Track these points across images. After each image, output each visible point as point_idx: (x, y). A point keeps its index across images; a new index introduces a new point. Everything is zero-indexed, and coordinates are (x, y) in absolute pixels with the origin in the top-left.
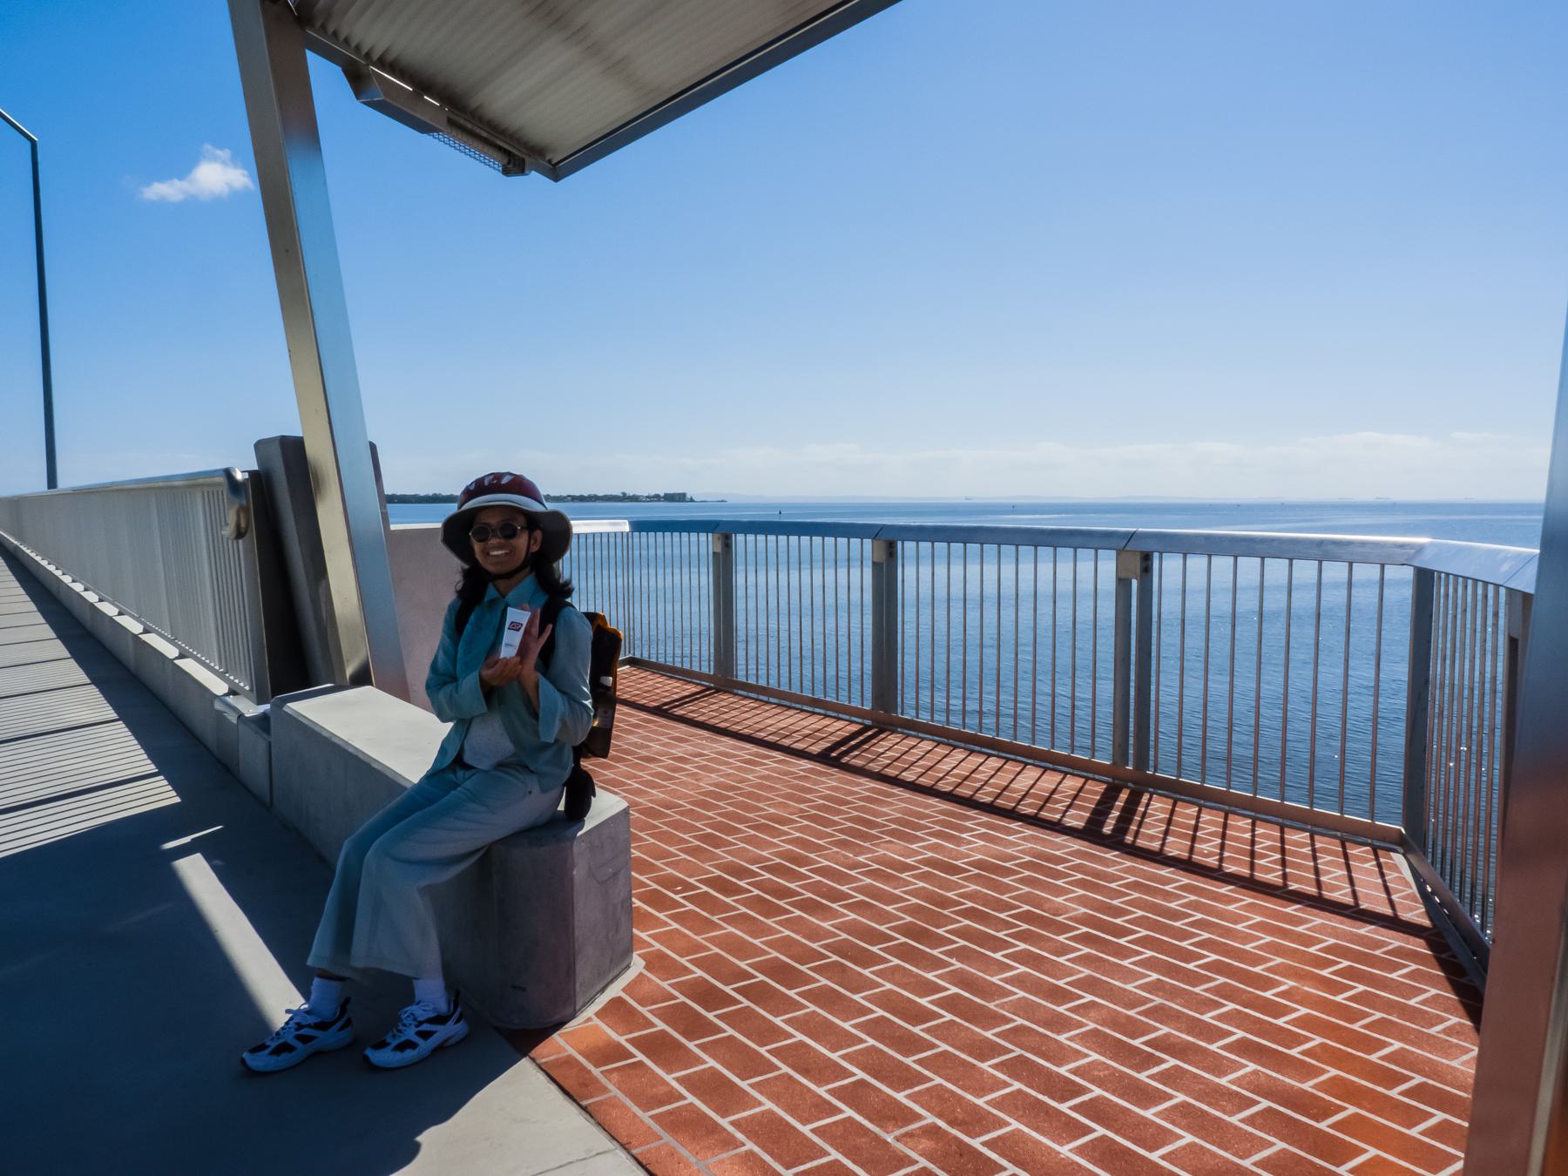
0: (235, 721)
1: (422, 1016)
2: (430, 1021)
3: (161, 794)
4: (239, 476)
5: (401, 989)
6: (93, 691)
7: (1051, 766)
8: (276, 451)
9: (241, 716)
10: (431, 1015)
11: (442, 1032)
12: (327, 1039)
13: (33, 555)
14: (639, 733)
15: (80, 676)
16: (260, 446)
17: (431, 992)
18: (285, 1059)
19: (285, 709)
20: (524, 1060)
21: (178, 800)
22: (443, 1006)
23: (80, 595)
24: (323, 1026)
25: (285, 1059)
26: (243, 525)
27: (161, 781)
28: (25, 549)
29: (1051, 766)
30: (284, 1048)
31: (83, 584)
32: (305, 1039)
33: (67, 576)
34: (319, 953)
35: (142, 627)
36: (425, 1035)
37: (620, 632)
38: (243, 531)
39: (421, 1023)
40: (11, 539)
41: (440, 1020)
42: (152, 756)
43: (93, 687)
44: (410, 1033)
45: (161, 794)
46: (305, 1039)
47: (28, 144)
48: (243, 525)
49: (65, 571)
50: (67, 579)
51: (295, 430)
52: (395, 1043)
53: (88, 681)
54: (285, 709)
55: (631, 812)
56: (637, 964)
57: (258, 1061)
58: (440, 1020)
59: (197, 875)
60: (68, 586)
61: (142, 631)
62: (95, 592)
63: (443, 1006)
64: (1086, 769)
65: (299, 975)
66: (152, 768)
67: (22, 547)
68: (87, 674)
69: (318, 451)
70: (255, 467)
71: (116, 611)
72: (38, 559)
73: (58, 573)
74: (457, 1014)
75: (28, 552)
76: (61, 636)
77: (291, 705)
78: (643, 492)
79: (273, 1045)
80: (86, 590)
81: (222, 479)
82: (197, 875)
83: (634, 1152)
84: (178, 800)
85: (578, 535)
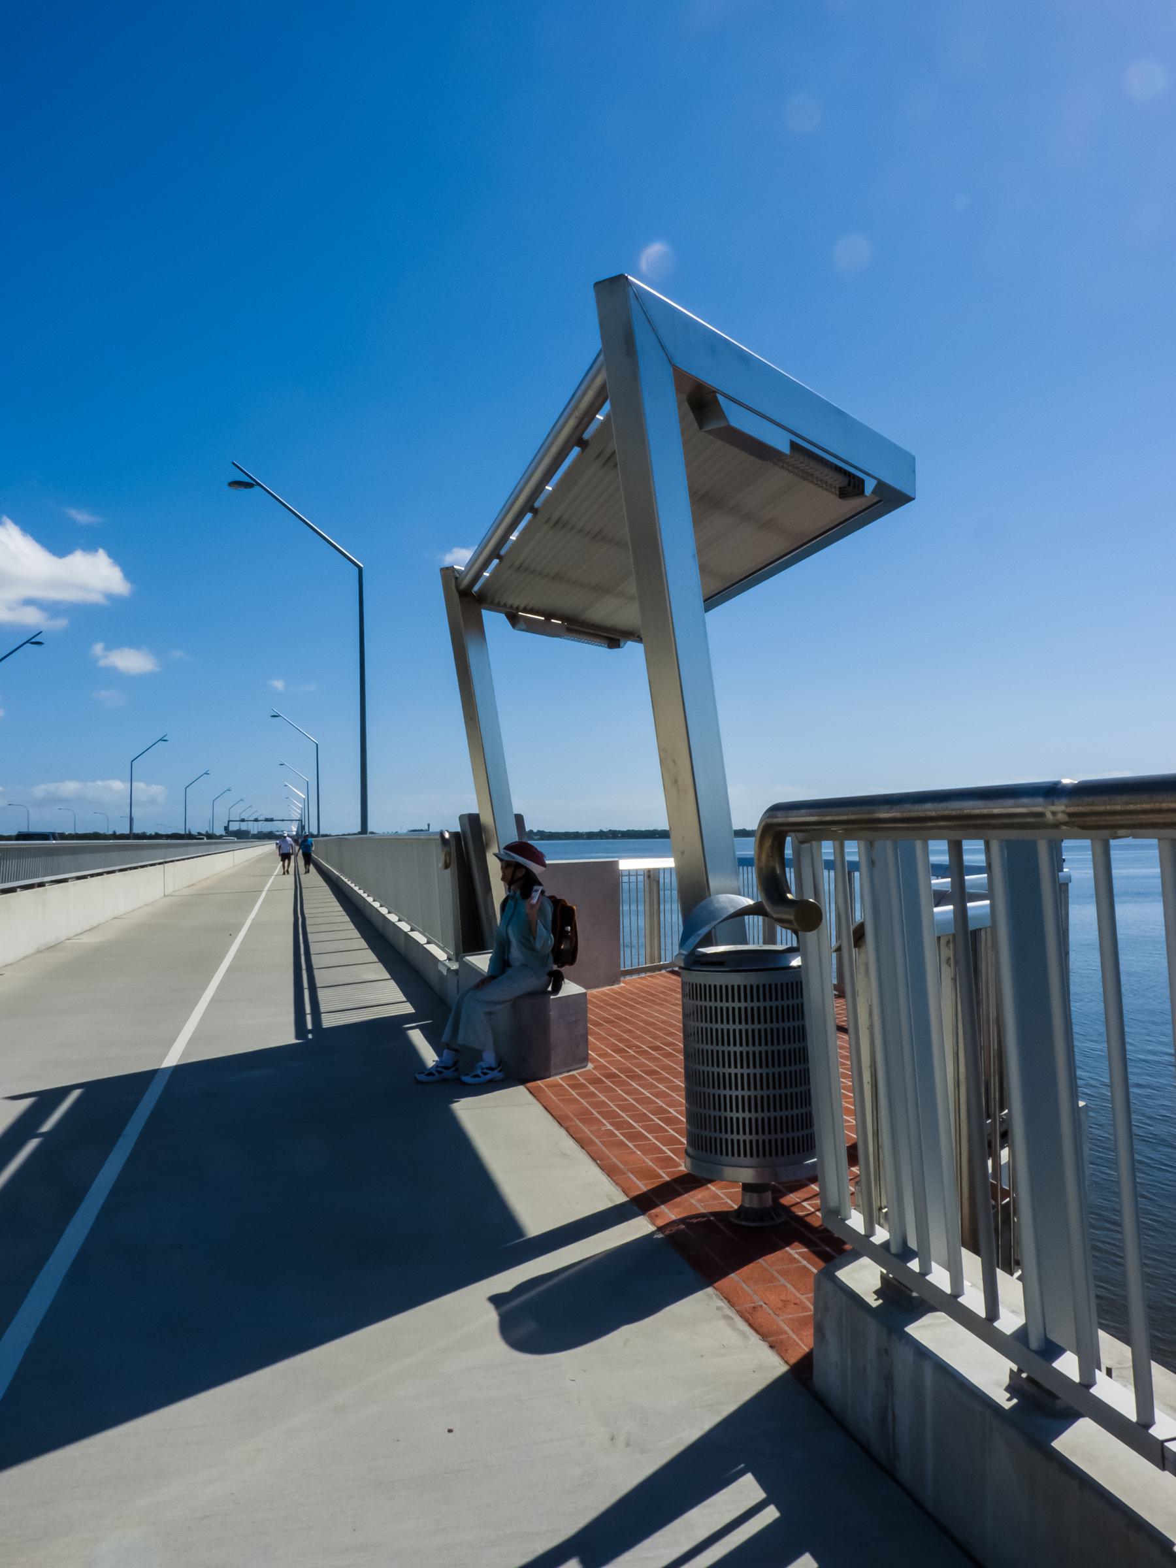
0: (445, 974)
1: (484, 1066)
2: (488, 1068)
3: (408, 1009)
4: (447, 835)
5: (477, 1055)
6: (380, 966)
8: (466, 821)
9: (449, 969)
10: (487, 1066)
11: (492, 1075)
12: (448, 1074)
13: (349, 883)
14: (842, 1038)
15: (374, 958)
16: (461, 817)
17: (489, 1058)
18: (431, 1078)
19: (464, 959)
20: (641, 1218)
21: (414, 1011)
22: (494, 1065)
23: (396, 926)
24: (446, 1068)
25: (431, 1078)
26: (448, 861)
27: (408, 1005)
28: (343, 878)
30: (430, 1074)
31: (387, 908)
32: (439, 1072)
33: (384, 908)
34: (446, 1037)
35: (410, 927)
36: (485, 1074)
37: (301, 855)
38: (448, 864)
39: (483, 1069)
40: (334, 871)
41: (491, 1069)
42: (405, 995)
43: (380, 963)
44: (479, 1072)
45: (408, 1009)
46: (439, 1072)
47: (357, 570)
48: (448, 861)
49: (383, 904)
50: (370, 900)
51: (475, 810)
52: (472, 1075)
53: (377, 961)
54: (464, 959)
55: (854, 1121)
56: (590, 1066)
57: (421, 1077)
58: (491, 1069)
59: (416, 1037)
60: (370, 904)
61: (426, 942)
62: (395, 914)
63: (494, 1065)
65: (438, 1051)
66: (405, 999)
67: (342, 877)
68: (390, 974)
69: (486, 819)
70: (458, 829)
71: (397, 918)
72: (352, 885)
73: (365, 895)
74: (499, 1069)
75: (346, 880)
76: (382, 960)
77: (467, 958)
78: (117, 874)
79: (426, 1072)
80: (381, 906)
81: (438, 837)
82: (416, 1037)
83: (614, 1178)
84: (414, 1011)
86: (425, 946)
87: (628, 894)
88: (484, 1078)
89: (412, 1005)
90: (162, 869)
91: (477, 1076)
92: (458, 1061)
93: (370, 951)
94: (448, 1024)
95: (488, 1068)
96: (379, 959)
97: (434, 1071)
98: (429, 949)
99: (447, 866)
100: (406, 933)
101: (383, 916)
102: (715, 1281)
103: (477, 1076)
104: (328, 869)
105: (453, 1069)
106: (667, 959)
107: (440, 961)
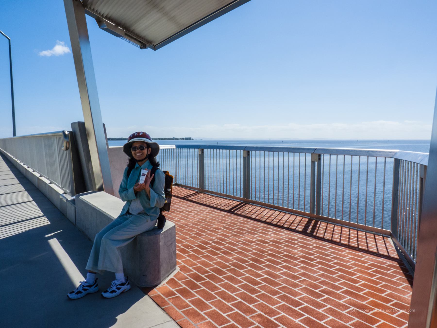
0: (65, 201)
1: (118, 283)
3: (45, 222)
4: (67, 133)
5: (112, 276)
6: (26, 193)
7: (293, 214)
10: (120, 283)
11: (123, 288)
13: (9, 155)
15: (22, 189)
17: (120, 277)
18: (80, 295)
19: (79, 198)
20: (146, 296)
21: (49, 223)
22: (123, 281)
24: (90, 286)
25: (80, 295)
26: (68, 146)
27: (45, 218)
28: (7, 153)
29: (293, 214)
30: (79, 292)
31: (27, 166)
32: (85, 290)
34: (89, 266)
38: (68, 148)
39: (117, 285)
41: (123, 284)
43: (26, 191)
44: (114, 288)
45: (45, 222)
46: (85, 290)
47: (8, 40)
48: (68, 146)
49: (18, 159)
50: (19, 162)
51: (82, 120)
52: (110, 291)
53: (25, 190)
57: (72, 296)
58: (123, 284)
63: (123, 281)
64: (303, 215)
66: (42, 214)
69: (88, 126)
70: (71, 130)
72: (11, 156)
73: (16, 160)
75: (8, 154)
79: (76, 291)
80: (24, 164)
81: (62, 134)
83: (177, 321)
85: (161, 149)
86: (49, 185)
87: (301, 180)
88: (119, 292)
89: (36, 202)
90: (288, 154)
91: (114, 291)
92: (97, 279)
93: (20, 185)
94: (90, 257)
95: (120, 285)
96: (20, 182)
97: (81, 290)
98: (41, 179)
99: (67, 149)
100: (38, 178)
101: (26, 169)
102: (148, 293)
103: (114, 291)
104: (271, 272)
105: (94, 286)
106: (333, 239)
107: (60, 194)
